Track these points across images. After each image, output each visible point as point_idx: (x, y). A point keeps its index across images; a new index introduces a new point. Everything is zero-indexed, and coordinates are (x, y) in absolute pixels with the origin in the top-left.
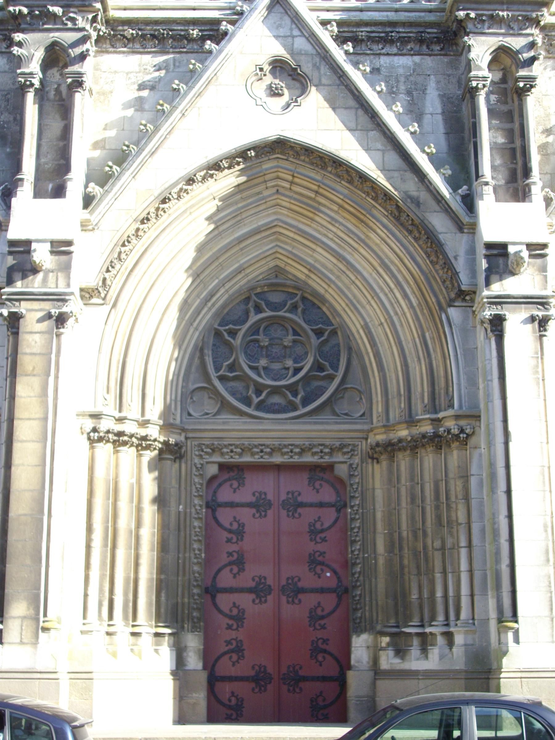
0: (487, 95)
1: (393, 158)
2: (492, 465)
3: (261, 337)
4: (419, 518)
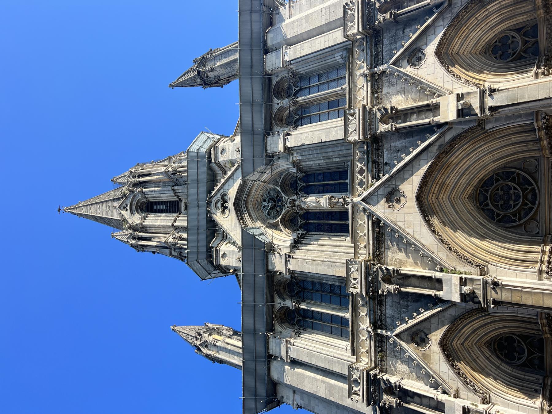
3: (499, 204)
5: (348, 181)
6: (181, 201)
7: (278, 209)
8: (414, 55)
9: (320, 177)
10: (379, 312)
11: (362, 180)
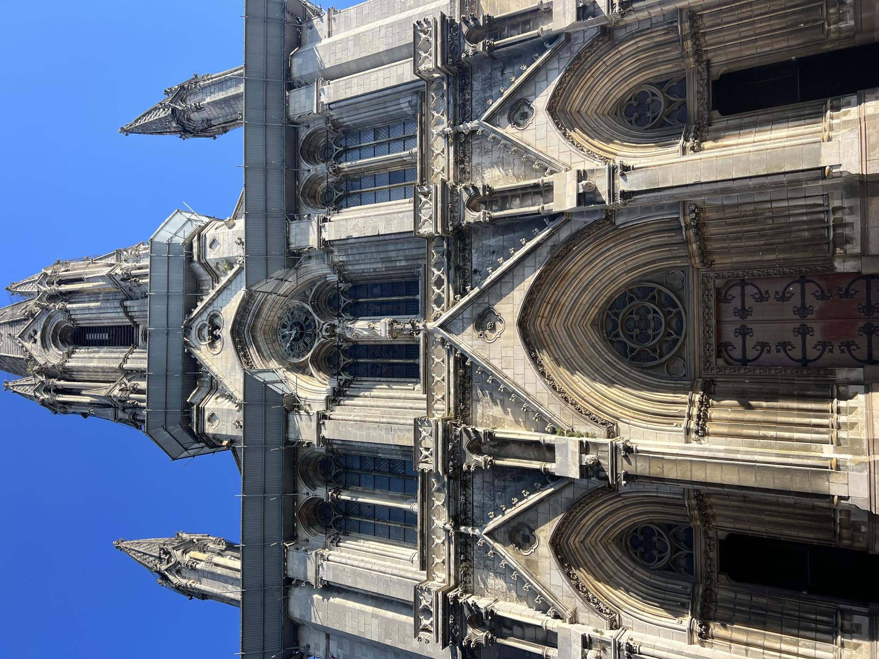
0: (493, 211)
1: (529, 262)
2: (715, 192)
3: (634, 333)
4: (751, 234)
5: (419, 297)
6: (138, 326)
7: (307, 340)
8: (517, 109)
9: (376, 291)
10: (462, 498)
11: (439, 295)
